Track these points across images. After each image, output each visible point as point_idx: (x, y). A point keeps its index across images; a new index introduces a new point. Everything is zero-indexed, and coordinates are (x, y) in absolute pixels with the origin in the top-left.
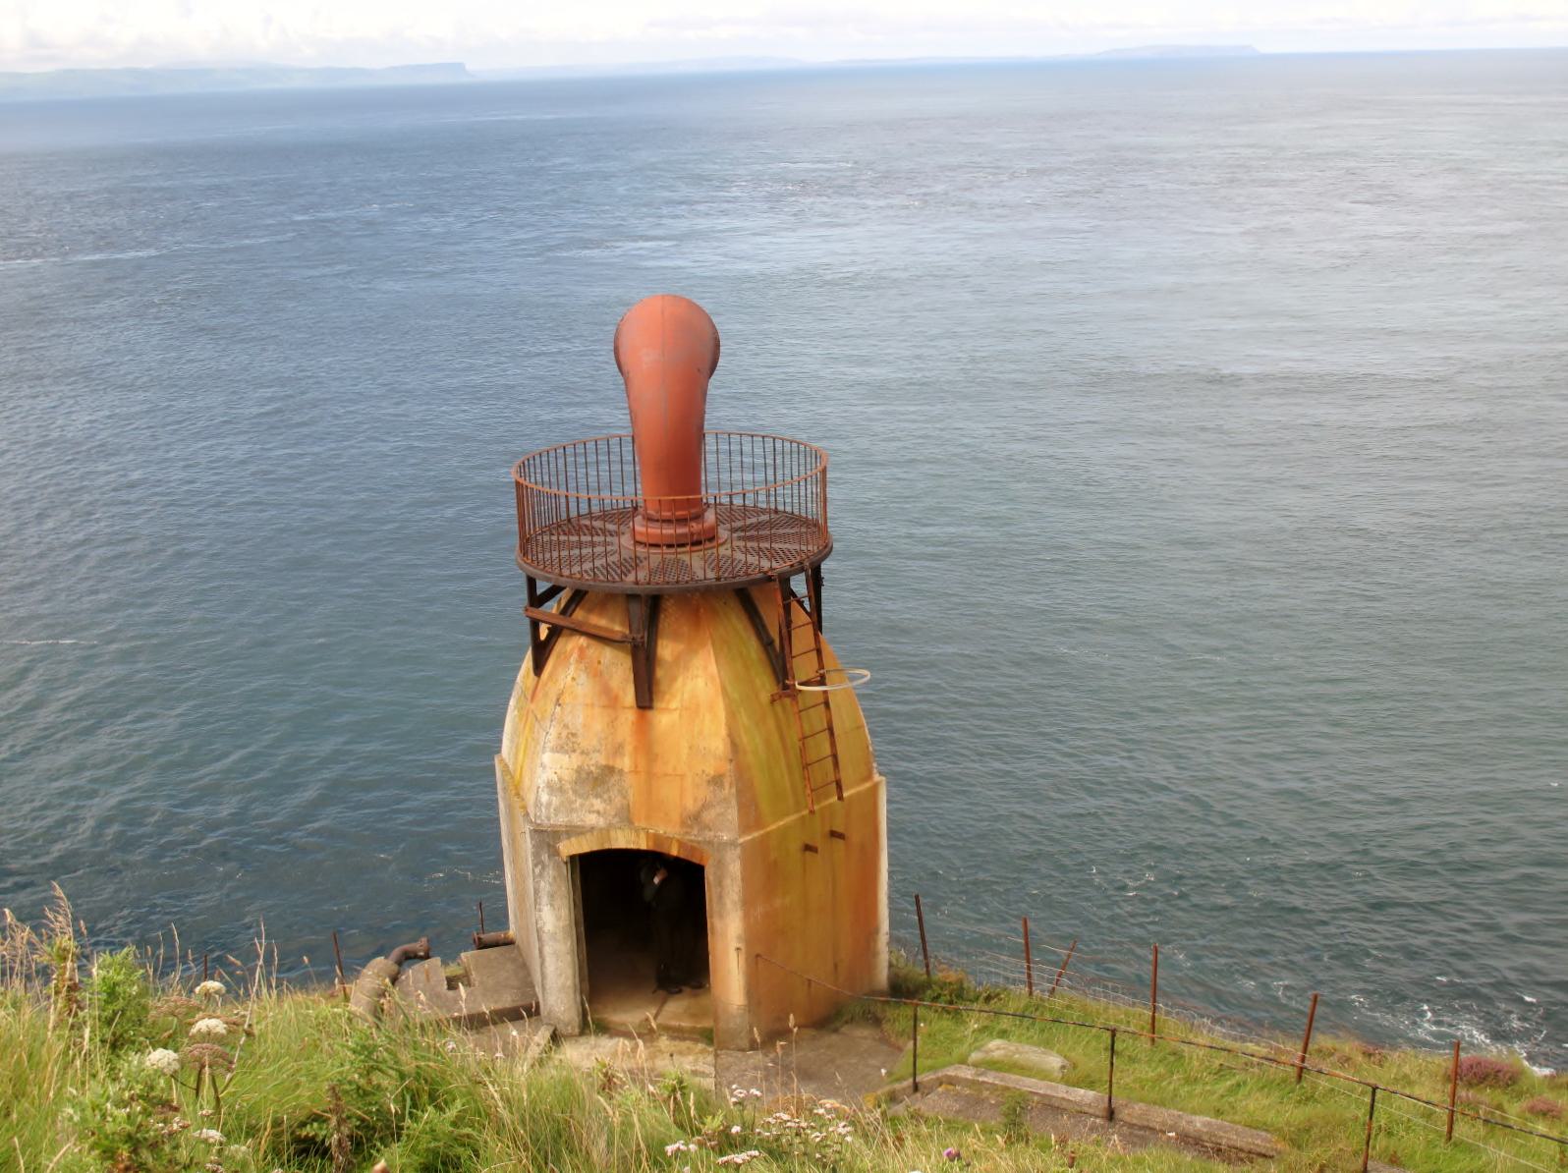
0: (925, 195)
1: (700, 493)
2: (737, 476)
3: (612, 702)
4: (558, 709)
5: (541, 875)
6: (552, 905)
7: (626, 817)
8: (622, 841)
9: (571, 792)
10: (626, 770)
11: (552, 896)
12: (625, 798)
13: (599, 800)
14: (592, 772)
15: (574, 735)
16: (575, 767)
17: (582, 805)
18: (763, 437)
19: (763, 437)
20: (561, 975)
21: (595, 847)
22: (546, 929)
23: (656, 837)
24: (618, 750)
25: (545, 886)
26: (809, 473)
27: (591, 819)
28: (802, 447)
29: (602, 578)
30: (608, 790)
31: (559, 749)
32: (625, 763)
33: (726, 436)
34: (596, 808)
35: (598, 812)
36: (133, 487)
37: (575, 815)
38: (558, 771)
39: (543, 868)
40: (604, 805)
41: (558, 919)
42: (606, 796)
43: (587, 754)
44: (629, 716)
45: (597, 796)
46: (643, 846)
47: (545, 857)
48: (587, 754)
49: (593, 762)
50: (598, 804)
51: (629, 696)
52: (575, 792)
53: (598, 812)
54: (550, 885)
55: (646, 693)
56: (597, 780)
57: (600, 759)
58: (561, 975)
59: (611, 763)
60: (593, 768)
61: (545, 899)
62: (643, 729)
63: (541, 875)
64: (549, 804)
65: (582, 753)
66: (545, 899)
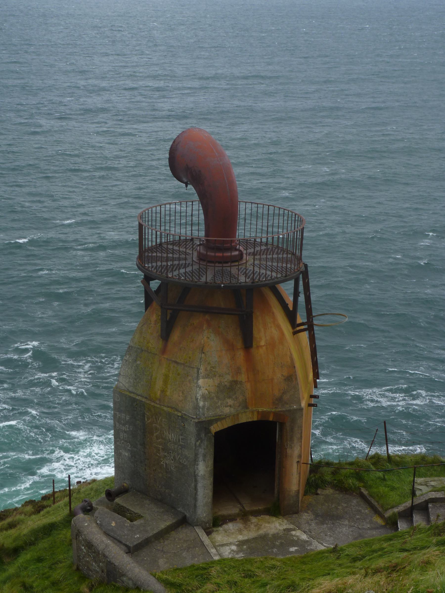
0: (142, 55)
1: (235, 237)
2: (275, 230)
3: (231, 347)
4: (203, 355)
5: (200, 446)
6: (204, 460)
7: (245, 405)
8: (244, 418)
9: (215, 398)
10: (244, 381)
11: (205, 456)
12: (244, 396)
13: (230, 400)
14: (226, 385)
15: (213, 367)
16: (217, 385)
17: (221, 404)
18: (284, 209)
19: (279, 208)
20: (205, 497)
21: (230, 425)
22: (200, 474)
23: (263, 413)
24: (238, 371)
25: (201, 451)
26: (296, 229)
27: (227, 410)
28: (290, 213)
29: (196, 280)
30: (235, 394)
31: (207, 376)
32: (243, 377)
33: (262, 206)
34: (229, 404)
35: (230, 406)
36: (150, 198)
37: (218, 410)
38: (208, 388)
39: (201, 442)
40: (233, 402)
41: (207, 467)
42: (234, 397)
43: (222, 376)
44: (240, 354)
45: (229, 397)
46: (255, 419)
47: (203, 435)
48: (222, 376)
49: (226, 380)
50: (230, 402)
51: (239, 344)
52: (218, 398)
53: (230, 406)
54: (204, 449)
55: (248, 341)
56: (229, 389)
57: (228, 378)
58: (205, 497)
59: (235, 379)
60: (226, 383)
61: (201, 458)
62: (249, 359)
63: (200, 446)
64: (204, 406)
65: (220, 376)
66: (201, 458)
